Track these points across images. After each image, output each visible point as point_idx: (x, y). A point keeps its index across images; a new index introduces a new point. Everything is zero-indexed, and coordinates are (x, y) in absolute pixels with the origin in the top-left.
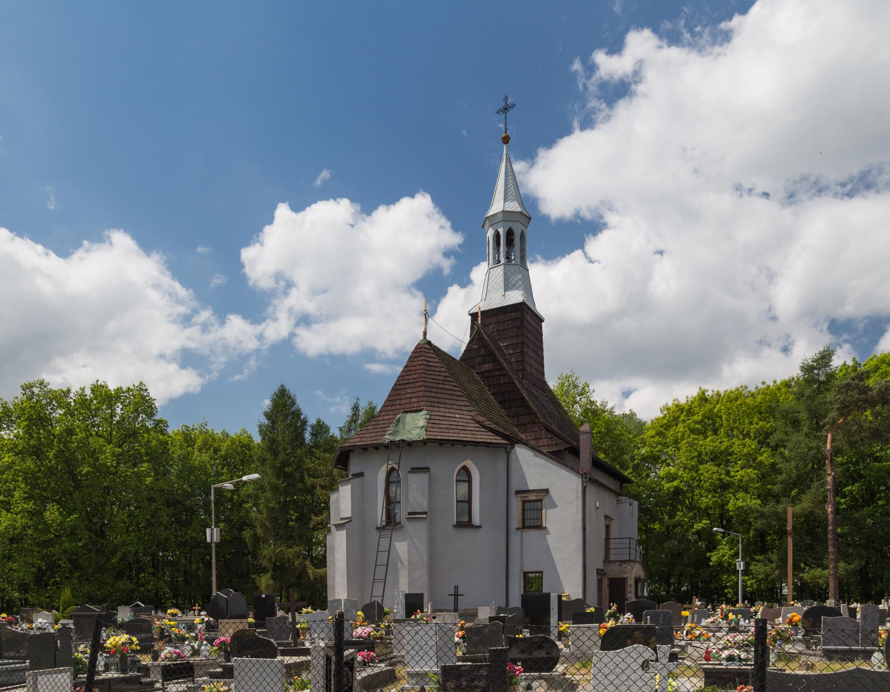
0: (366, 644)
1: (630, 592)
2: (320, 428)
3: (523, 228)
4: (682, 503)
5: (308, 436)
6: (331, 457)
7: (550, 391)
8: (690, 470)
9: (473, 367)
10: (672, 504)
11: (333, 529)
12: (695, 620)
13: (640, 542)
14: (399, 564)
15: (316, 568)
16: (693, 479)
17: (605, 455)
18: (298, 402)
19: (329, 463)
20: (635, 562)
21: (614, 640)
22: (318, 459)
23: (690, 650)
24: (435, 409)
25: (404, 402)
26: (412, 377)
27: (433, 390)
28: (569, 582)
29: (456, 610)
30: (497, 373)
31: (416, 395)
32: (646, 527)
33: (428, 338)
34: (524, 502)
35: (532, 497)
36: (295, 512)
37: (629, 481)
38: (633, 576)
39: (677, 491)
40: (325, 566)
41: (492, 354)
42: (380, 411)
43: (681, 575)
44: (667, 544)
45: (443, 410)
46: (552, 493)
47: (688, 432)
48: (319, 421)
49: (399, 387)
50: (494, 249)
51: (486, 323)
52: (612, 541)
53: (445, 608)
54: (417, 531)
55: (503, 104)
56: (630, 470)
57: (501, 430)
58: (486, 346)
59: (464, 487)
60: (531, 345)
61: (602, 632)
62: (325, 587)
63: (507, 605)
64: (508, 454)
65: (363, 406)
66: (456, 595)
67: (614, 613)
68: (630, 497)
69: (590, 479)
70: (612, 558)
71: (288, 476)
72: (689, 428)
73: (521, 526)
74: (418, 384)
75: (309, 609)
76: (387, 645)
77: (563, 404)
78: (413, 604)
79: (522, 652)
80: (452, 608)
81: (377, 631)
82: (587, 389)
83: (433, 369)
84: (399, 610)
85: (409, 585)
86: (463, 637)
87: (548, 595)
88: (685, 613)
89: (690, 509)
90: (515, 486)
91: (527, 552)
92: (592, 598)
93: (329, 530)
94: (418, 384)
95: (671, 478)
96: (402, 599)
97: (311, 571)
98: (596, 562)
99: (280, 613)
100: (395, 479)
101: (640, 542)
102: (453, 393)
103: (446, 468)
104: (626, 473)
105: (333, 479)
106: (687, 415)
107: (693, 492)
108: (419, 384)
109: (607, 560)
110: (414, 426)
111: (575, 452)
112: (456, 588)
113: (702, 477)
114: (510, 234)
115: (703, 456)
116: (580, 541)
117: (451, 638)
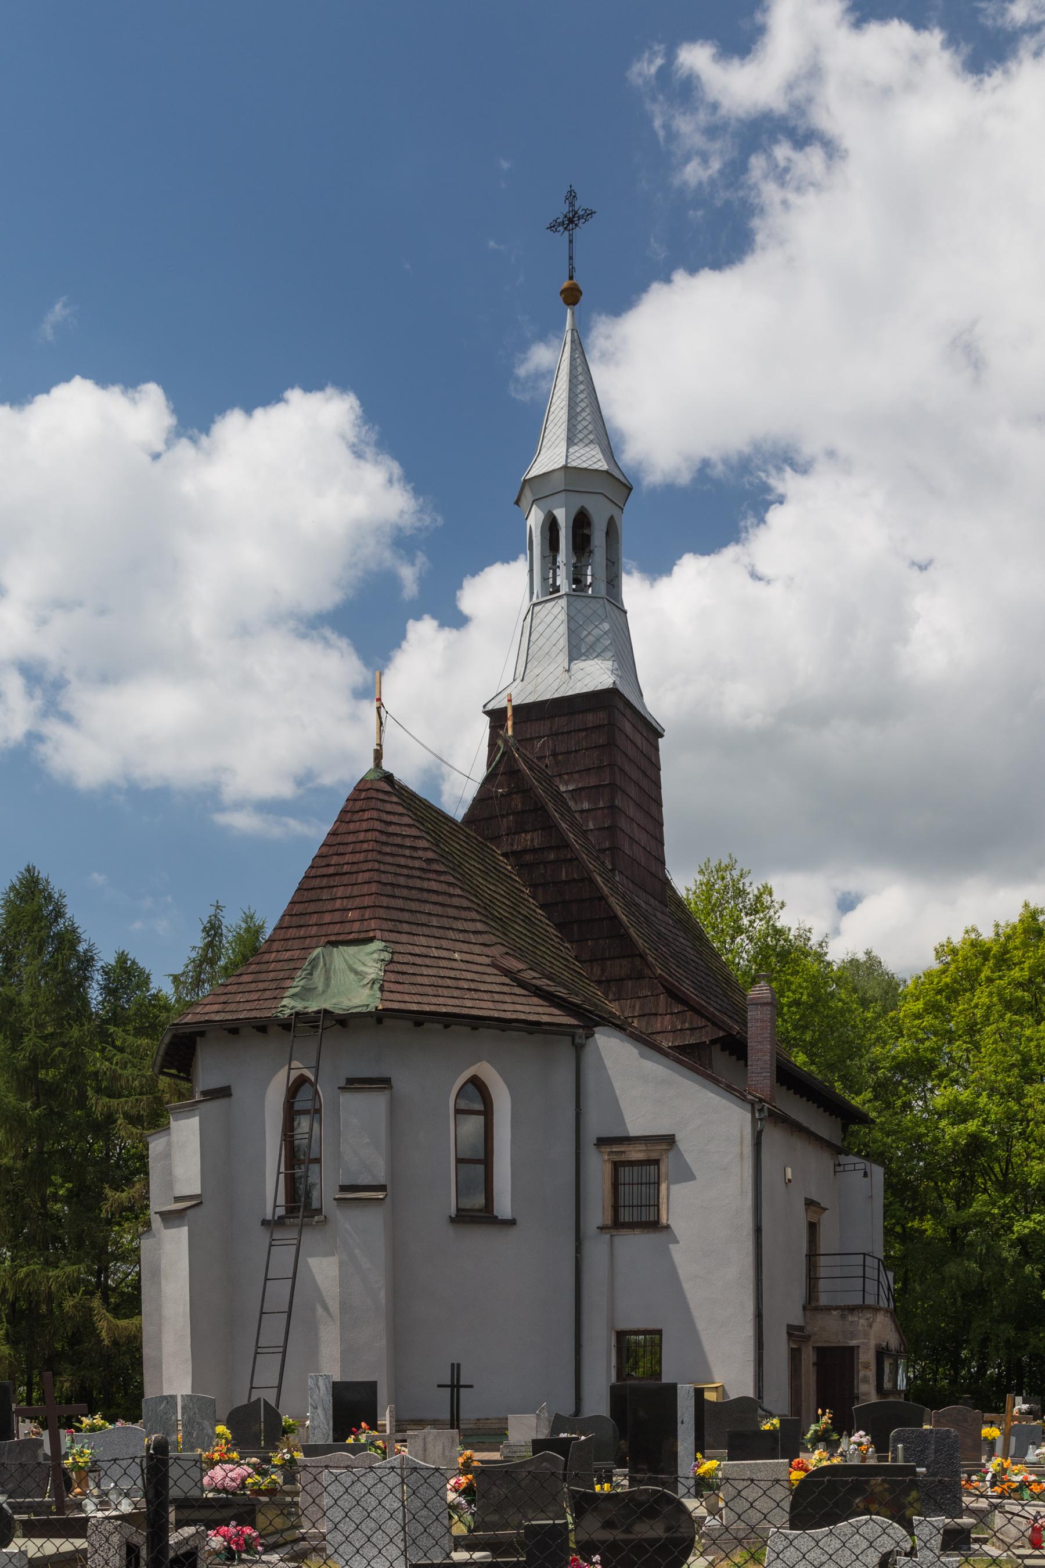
0: (235, 1507)
1: (866, 1380)
2: (126, 975)
3: (614, 511)
4: (987, 1172)
5: (95, 994)
6: (153, 1047)
7: (678, 902)
8: (1002, 1095)
9: (495, 839)
10: (963, 1174)
11: (156, 1222)
12: (1012, 1451)
13: (888, 1264)
14: (320, 1310)
15: (117, 1316)
16: (1011, 1117)
17: (807, 1056)
18: (69, 912)
19: (148, 1061)
20: (876, 1309)
21: (819, 1503)
22: (121, 1050)
23: (998, 1520)
24: (404, 938)
25: (327, 918)
26: (347, 858)
27: (397, 892)
28: (723, 1357)
29: (454, 1422)
30: (552, 856)
31: (357, 902)
32: (903, 1227)
33: (387, 766)
34: (616, 1166)
35: (636, 1154)
36: (66, 1179)
37: (863, 1119)
38: (873, 1343)
39: (976, 1144)
40: (140, 1313)
41: (540, 809)
42: (271, 940)
43: (985, 1341)
44: (952, 1268)
45: (423, 941)
46: (682, 1144)
47: (999, 1007)
48: (122, 958)
49: (317, 883)
50: (543, 557)
51: (525, 732)
52: (823, 1261)
53: (429, 1415)
54: (362, 1230)
55: (565, 209)
56: (868, 1094)
57: (561, 992)
58: (527, 792)
59: (473, 1125)
60: (633, 791)
61: (797, 1475)
62: (138, 1363)
63: (578, 1411)
64: (579, 1049)
65: (232, 922)
66: (455, 1387)
67: (826, 1431)
68: (867, 1157)
69: (771, 1114)
70: (824, 1300)
71: (47, 1092)
72: (1001, 998)
73: (609, 1222)
74: (361, 877)
75: (98, 1420)
76: (289, 1510)
77: (710, 933)
78: (352, 1407)
79: (608, 1525)
80: (447, 1416)
81: (264, 1473)
82: (766, 899)
83: (398, 840)
84: (316, 1421)
85: (343, 1359)
86: (467, 1492)
87: (673, 1387)
88: (990, 1432)
89: (1004, 1187)
90: (596, 1126)
91: (625, 1284)
92: (778, 1397)
93: (148, 1224)
94: (361, 877)
95: (961, 1113)
96: (324, 1395)
97: (105, 1324)
98: (787, 1308)
99: (25, 1429)
100: (308, 1105)
101: (888, 1264)
102: (447, 900)
103: (433, 1081)
104: (857, 1101)
105: (159, 1100)
106: (997, 967)
107: (1009, 1147)
108: (366, 876)
109: (811, 1304)
110: (353, 978)
111: (736, 1047)
112: (456, 1369)
113: (1031, 1114)
114: (581, 522)
115: (1033, 1064)
116: (749, 1260)
117: (439, 1493)
